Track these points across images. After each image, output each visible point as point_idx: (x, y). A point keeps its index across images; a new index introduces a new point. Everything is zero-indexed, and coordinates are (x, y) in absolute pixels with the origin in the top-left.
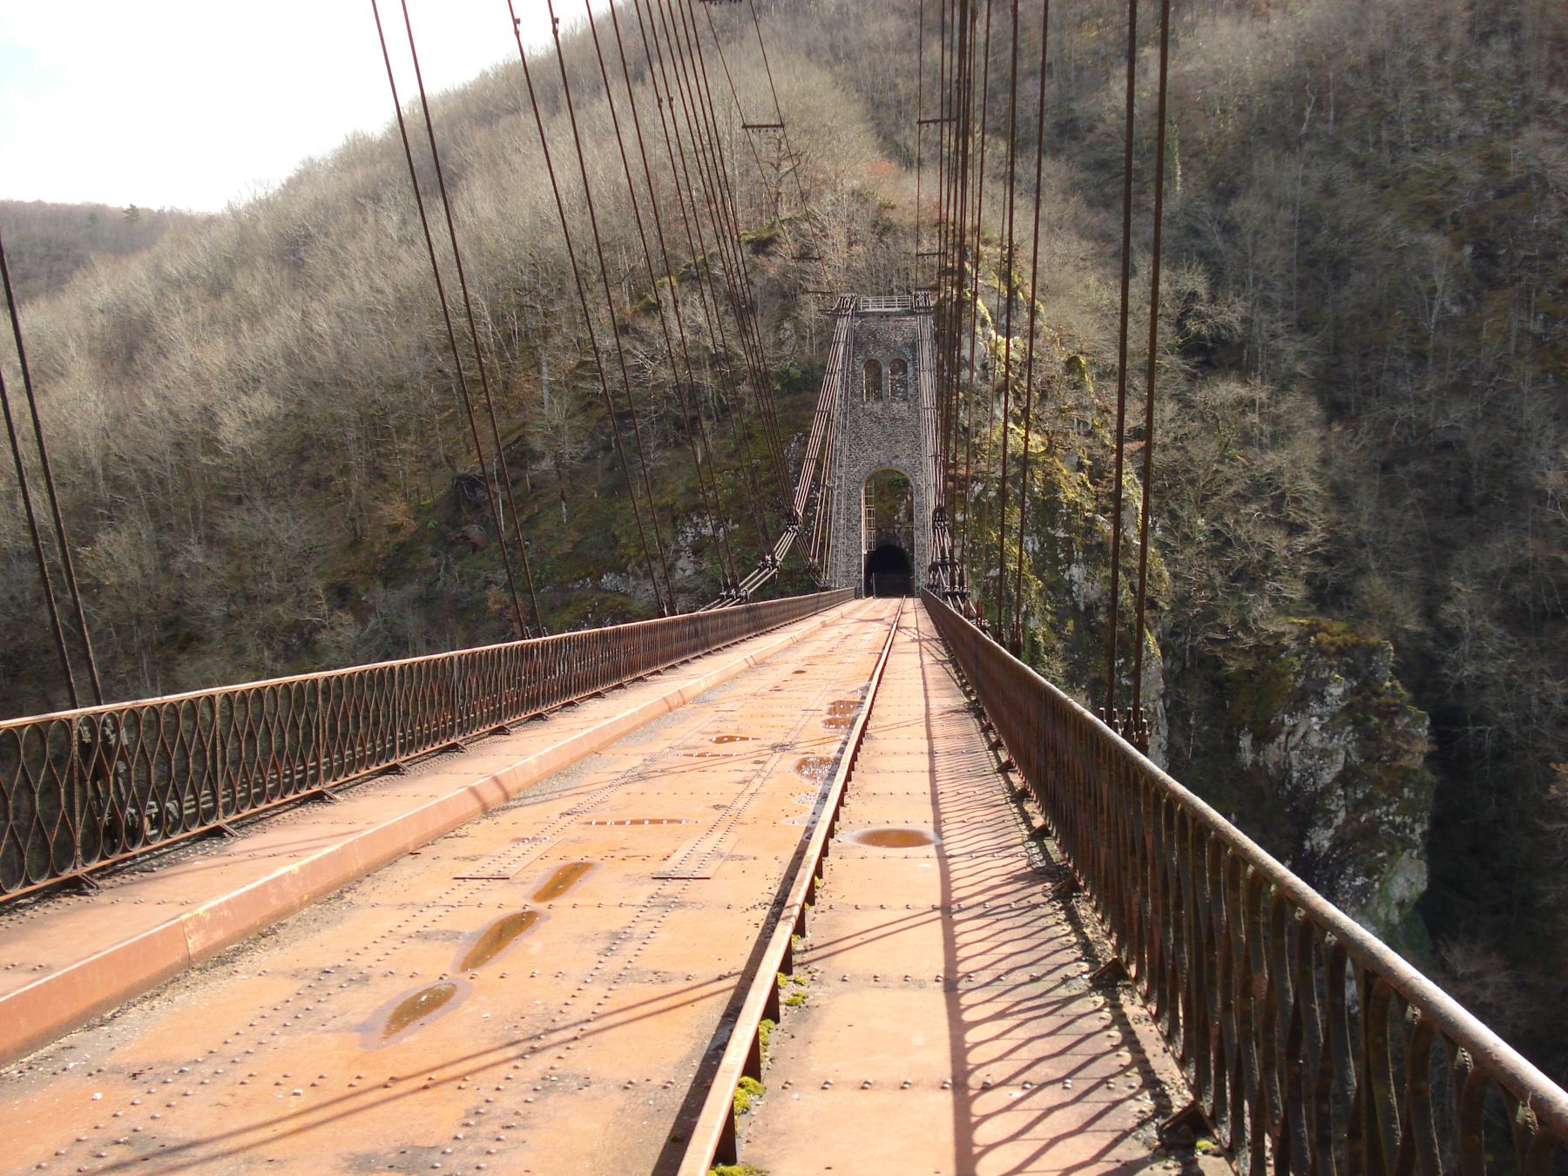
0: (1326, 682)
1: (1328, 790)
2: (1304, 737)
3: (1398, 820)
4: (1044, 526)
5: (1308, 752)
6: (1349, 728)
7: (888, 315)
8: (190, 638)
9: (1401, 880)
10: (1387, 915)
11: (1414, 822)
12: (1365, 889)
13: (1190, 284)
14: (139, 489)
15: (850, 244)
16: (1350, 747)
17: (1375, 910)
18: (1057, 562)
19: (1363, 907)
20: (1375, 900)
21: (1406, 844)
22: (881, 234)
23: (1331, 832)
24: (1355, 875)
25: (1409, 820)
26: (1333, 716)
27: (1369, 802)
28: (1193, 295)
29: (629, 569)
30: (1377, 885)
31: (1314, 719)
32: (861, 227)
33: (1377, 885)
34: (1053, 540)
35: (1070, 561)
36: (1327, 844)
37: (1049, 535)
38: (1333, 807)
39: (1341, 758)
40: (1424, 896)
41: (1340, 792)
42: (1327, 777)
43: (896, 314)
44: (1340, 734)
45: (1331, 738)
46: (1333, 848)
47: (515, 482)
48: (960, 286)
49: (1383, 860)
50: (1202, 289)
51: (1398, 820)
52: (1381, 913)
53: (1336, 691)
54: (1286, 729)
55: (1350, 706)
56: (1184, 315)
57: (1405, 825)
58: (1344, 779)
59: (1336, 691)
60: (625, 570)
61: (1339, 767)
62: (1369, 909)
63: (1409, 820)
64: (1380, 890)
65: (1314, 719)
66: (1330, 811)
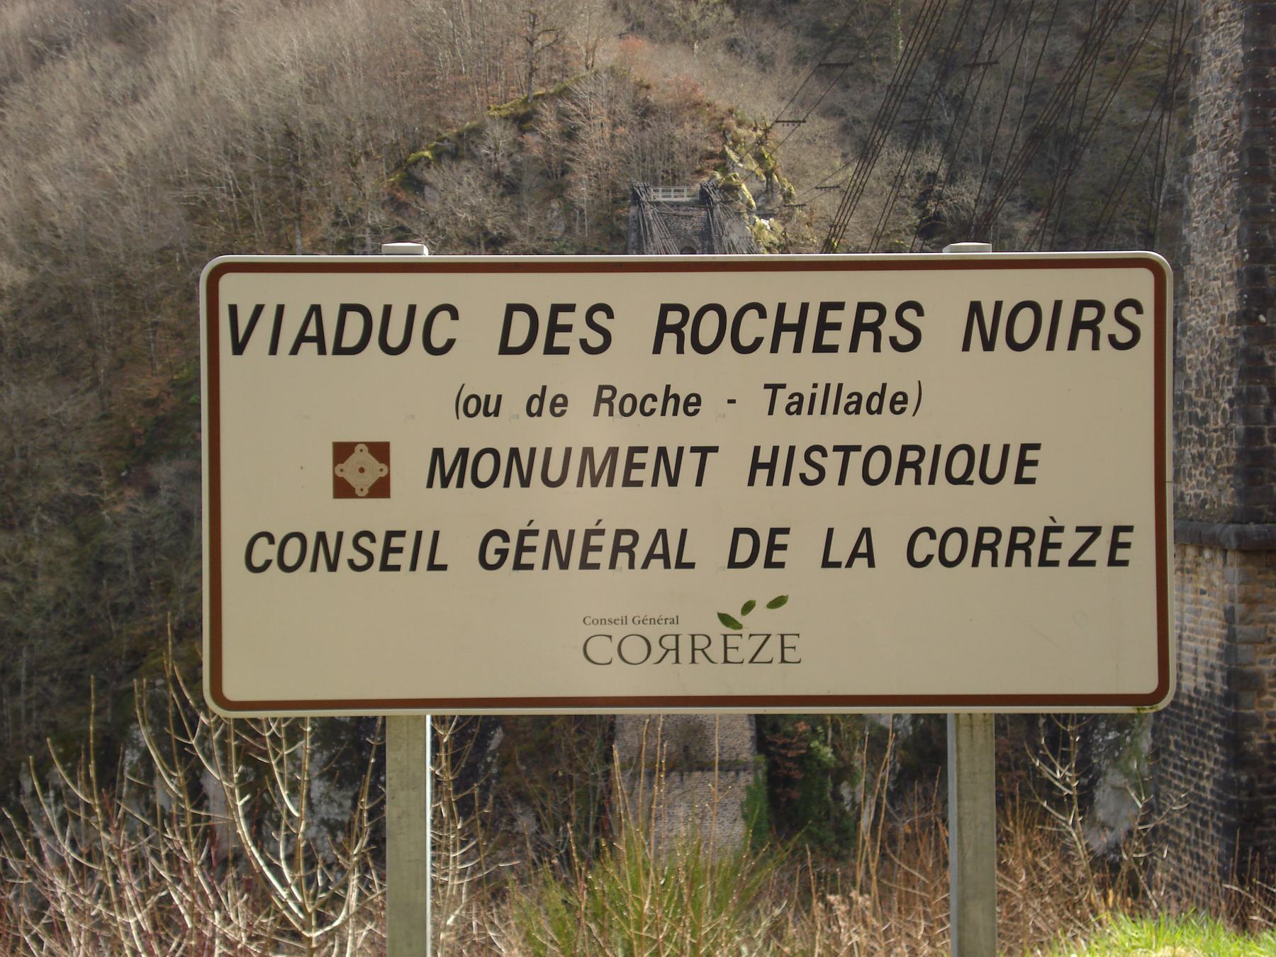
7: (678, 205)
8: (499, 894)
12: (1117, 743)
13: (929, 164)
14: (482, 781)
15: (614, 126)
19: (1116, 759)
20: (1126, 755)
22: (644, 115)
24: (1108, 730)
28: (933, 176)
30: (1128, 739)
32: (622, 107)
33: (1128, 739)
43: (686, 204)
48: (725, 171)
50: (942, 174)
56: (925, 195)
62: (1121, 762)
64: (1131, 745)
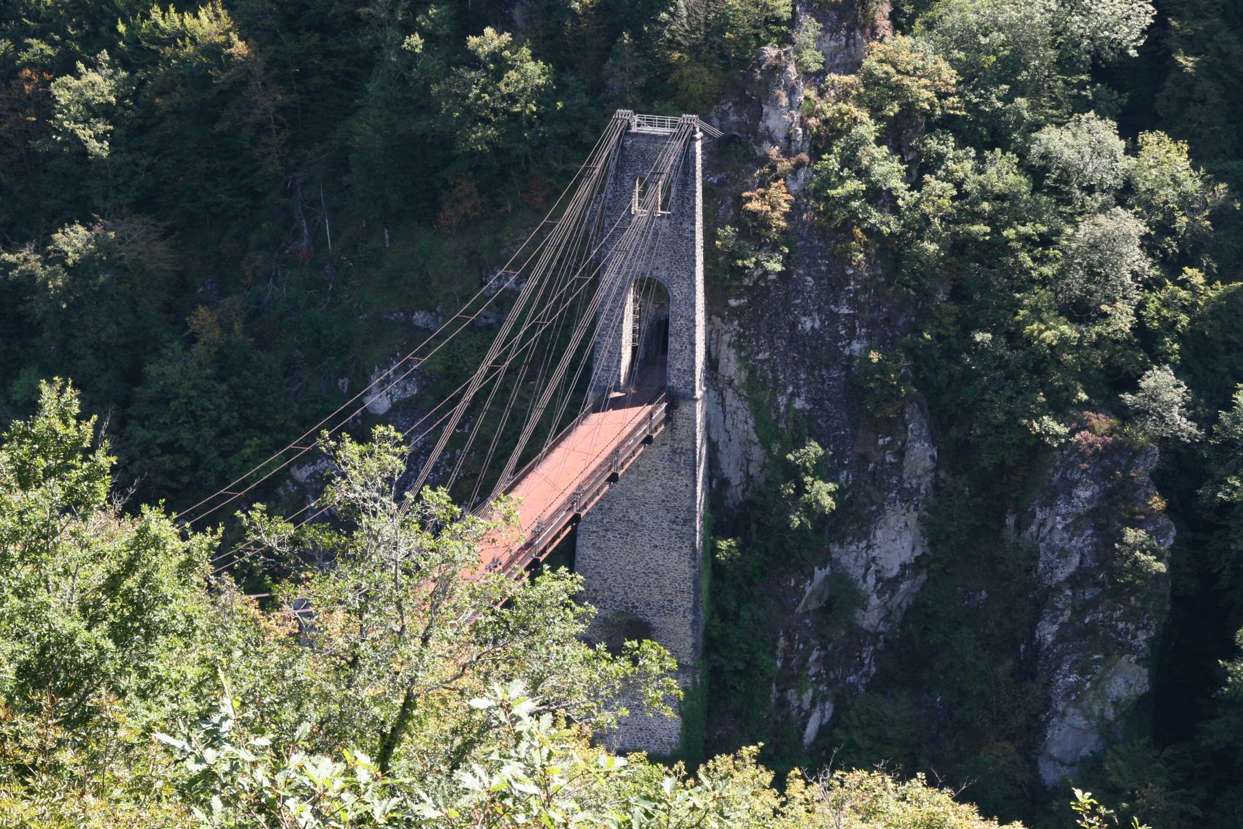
0: (1075, 484)
1: (1058, 588)
2: (1050, 532)
3: (1121, 625)
4: (827, 303)
5: (1051, 548)
6: (1089, 532)
9: (1120, 681)
10: (1102, 710)
11: (1137, 629)
12: (1077, 686)
16: (1086, 550)
17: (1090, 707)
18: (839, 338)
21: (1126, 648)
23: (1056, 628)
25: (1132, 627)
26: (1078, 517)
27: (1093, 604)
29: (438, 309)
31: (1059, 518)
34: (834, 317)
35: (852, 335)
36: (1050, 638)
37: (832, 312)
38: (1060, 606)
39: (1076, 560)
40: (1143, 700)
41: (1068, 592)
42: (1061, 575)
44: (1081, 536)
45: (1070, 540)
46: (1054, 644)
47: (183, 751)
49: (1097, 661)
51: (1121, 625)
52: (1096, 709)
53: (1083, 493)
54: (1036, 521)
55: (1095, 510)
57: (1127, 631)
58: (1075, 581)
59: (1083, 493)
60: (434, 310)
61: (1071, 569)
63: (1132, 627)
65: (1059, 518)
66: (1057, 609)
